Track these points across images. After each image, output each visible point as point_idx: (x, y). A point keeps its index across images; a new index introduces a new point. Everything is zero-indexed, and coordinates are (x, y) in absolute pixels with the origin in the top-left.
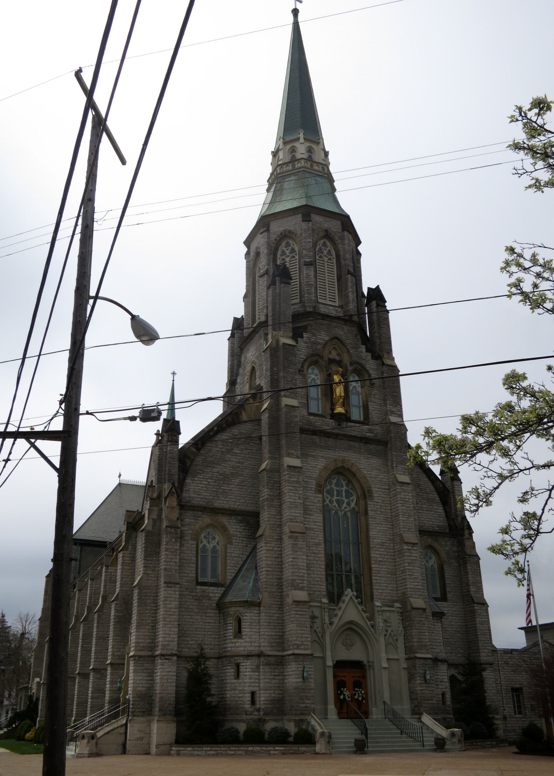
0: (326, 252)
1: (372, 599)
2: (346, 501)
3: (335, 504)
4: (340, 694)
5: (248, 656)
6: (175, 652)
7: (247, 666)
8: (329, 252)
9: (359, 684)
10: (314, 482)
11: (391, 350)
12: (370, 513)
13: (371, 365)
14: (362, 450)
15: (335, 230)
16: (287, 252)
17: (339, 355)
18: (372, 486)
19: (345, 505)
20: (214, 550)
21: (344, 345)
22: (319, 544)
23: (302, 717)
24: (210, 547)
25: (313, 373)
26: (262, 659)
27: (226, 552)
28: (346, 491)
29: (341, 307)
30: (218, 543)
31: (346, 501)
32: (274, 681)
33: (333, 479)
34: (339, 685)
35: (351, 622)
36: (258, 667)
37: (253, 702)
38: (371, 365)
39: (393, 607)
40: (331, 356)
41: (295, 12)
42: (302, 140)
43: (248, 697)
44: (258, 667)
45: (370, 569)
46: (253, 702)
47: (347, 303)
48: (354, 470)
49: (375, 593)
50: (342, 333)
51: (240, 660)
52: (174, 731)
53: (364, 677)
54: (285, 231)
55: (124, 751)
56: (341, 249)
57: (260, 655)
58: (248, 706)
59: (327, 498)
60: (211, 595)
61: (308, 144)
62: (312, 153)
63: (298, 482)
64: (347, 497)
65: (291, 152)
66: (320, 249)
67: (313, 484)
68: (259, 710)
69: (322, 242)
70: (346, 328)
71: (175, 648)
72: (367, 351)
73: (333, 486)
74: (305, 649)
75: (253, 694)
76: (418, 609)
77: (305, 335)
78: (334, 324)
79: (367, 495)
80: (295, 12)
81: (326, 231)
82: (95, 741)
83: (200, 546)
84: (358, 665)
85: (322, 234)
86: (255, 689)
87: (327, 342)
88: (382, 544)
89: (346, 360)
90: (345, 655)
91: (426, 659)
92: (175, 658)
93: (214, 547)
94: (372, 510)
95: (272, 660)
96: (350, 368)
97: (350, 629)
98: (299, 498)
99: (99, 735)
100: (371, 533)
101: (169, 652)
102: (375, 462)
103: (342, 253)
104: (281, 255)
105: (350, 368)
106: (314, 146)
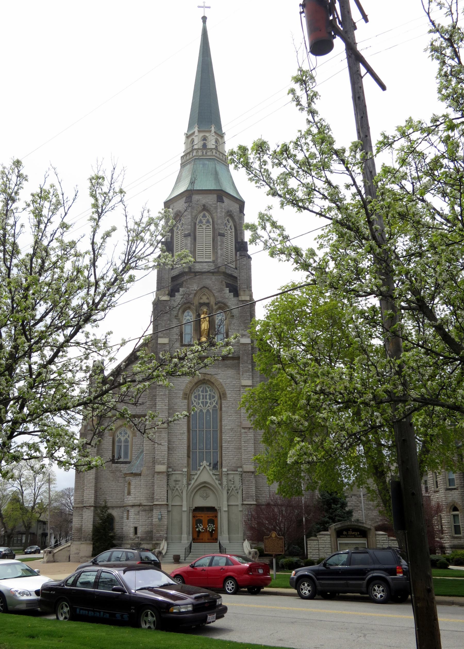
0: (204, 222)
1: (221, 467)
2: (209, 401)
3: (201, 404)
4: (197, 528)
5: (132, 506)
6: (93, 505)
7: (132, 511)
8: (208, 222)
9: (212, 521)
10: (181, 393)
11: (251, 287)
12: (224, 409)
13: (232, 301)
14: (220, 366)
15: (211, 203)
16: (204, 222)
17: (208, 298)
18: (227, 390)
19: (208, 404)
20: (126, 441)
21: (211, 291)
22: (183, 433)
23: (158, 542)
24: (123, 439)
25: (188, 315)
26: (141, 507)
27: (132, 442)
28: (210, 395)
29: (213, 262)
30: (129, 437)
31: (209, 401)
32: (147, 521)
33: (200, 387)
34: (197, 522)
35: (205, 482)
36: (139, 512)
37: (136, 532)
38: (232, 301)
39: (237, 471)
40: (202, 301)
41: (204, 19)
42: (196, 133)
43: (132, 530)
44: (139, 512)
45: (221, 447)
46: (136, 532)
47: (217, 259)
48: (212, 380)
49: (224, 462)
50: (210, 282)
51: (129, 508)
52: (91, 549)
53: (216, 517)
54: (177, 211)
55: (69, 561)
56: (215, 217)
57: (140, 505)
58: (132, 535)
59: (195, 401)
60: (122, 469)
61: (202, 134)
62: (206, 140)
63: (164, 395)
64: (210, 399)
65: (203, 140)
66: (201, 220)
67: (181, 394)
68: (138, 538)
69: (202, 214)
70: (214, 278)
71: (93, 502)
72: (230, 292)
73: (200, 393)
74: (162, 501)
75: (136, 529)
76: (248, 472)
77: (181, 289)
78: (204, 277)
79: (222, 396)
80: (204, 19)
81: (204, 205)
82: (52, 554)
83: (117, 439)
84: (212, 509)
85: (200, 209)
86: (136, 525)
87: (197, 292)
88: (232, 429)
89: (212, 301)
90: (200, 502)
91: (251, 505)
92: (92, 508)
93: (126, 439)
94: (225, 407)
95: (147, 508)
96: (215, 307)
97: (204, 486)
98: (165, 405)
99: (55, 551)
100: (223, 423)
101: (88, 505)
102: (230, 372)
103: (216, 220)
104: (199, 223)
105: (215, 307)
106: (207, 135)
